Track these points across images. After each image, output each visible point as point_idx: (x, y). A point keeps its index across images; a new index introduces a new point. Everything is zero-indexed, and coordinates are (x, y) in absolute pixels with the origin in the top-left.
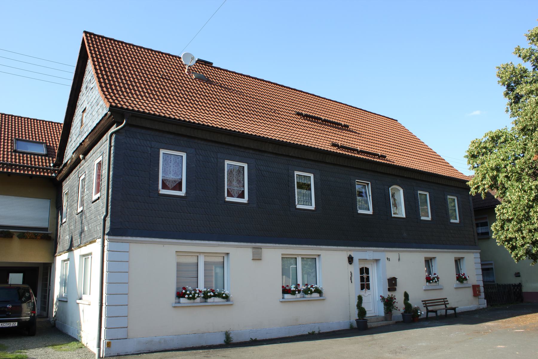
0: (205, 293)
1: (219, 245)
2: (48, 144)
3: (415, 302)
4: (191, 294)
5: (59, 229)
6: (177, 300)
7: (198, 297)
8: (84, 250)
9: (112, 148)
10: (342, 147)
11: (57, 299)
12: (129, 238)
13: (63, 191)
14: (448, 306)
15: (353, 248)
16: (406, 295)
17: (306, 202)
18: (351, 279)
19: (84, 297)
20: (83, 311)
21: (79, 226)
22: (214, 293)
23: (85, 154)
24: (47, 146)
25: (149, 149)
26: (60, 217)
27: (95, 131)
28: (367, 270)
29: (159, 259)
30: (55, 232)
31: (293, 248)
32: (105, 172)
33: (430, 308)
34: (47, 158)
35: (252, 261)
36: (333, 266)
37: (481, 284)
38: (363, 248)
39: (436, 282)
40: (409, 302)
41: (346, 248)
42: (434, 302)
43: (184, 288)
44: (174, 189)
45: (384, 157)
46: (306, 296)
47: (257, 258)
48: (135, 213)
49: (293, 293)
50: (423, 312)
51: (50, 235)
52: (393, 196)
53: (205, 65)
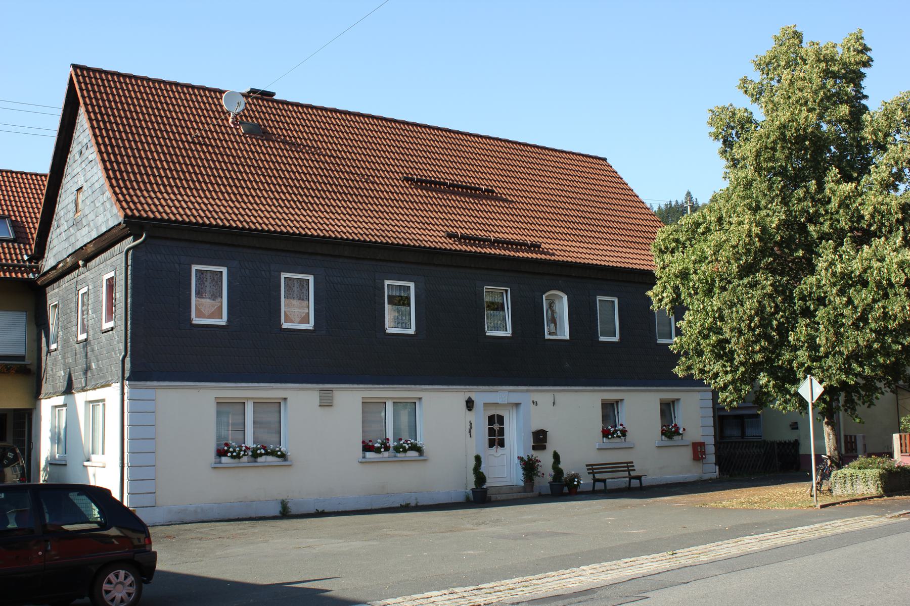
0: (254, 451)
1: (273, 388)
2: (13, 218)
3: (567, 467)
4: (235, 451)
5: (44, 358)
6: (218, 460)
7: (244, 455)
8: (92, 395)
9: (130, 267)
10: (465, 238)
11: (47, 461)
12: (155, 383)
13: (49, 302)
14: (633, 474)
15: (475, 387)
16: (556, 457)
17: (399, 323)
18: (470, 432)
19: (93, 457)
20: (94, 475)
21: (82, 362)
22: (266, 451)
23: (88, 260)
24: (12, 220)
25: (177, 266)
26: (44, 340)
27: (104, 238)
28: (501, 419)
29: (192, 408)
30: (35, 362)
31: (379, 390)
32: (119, 294)
33: (598, 476)
34: (16, 245)
35: (322, 410)
36: (444, 416)
37: (710, 441)
38: (491, 387)
39: (618, 437)
40: (560, 466)
41: (463, 387)
42: (613, 467)
43: (226, 445)
44: (211, 316)
45: (535, 247)
46: (398, 455)
47: (326, 403)
48: (160, 351)
49: (378, 450)
50: (586, 481)
51: (28, 367)
52: (551, 306)
53: (262, 100)
